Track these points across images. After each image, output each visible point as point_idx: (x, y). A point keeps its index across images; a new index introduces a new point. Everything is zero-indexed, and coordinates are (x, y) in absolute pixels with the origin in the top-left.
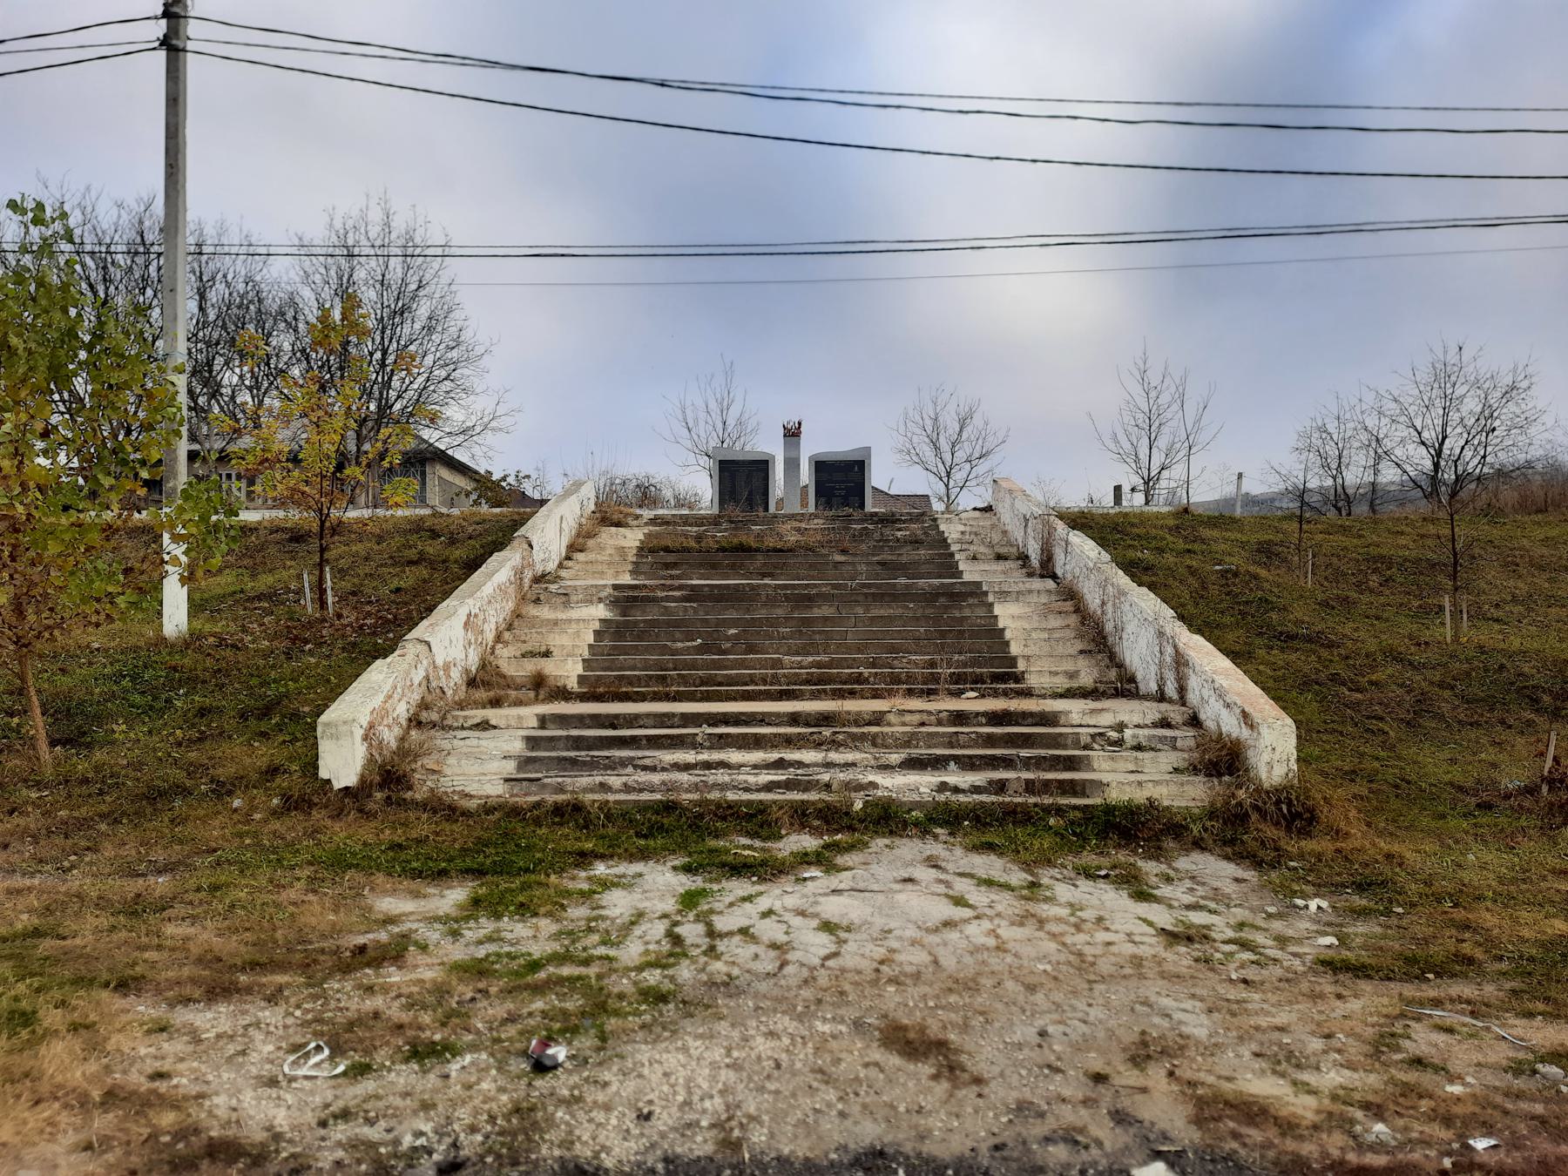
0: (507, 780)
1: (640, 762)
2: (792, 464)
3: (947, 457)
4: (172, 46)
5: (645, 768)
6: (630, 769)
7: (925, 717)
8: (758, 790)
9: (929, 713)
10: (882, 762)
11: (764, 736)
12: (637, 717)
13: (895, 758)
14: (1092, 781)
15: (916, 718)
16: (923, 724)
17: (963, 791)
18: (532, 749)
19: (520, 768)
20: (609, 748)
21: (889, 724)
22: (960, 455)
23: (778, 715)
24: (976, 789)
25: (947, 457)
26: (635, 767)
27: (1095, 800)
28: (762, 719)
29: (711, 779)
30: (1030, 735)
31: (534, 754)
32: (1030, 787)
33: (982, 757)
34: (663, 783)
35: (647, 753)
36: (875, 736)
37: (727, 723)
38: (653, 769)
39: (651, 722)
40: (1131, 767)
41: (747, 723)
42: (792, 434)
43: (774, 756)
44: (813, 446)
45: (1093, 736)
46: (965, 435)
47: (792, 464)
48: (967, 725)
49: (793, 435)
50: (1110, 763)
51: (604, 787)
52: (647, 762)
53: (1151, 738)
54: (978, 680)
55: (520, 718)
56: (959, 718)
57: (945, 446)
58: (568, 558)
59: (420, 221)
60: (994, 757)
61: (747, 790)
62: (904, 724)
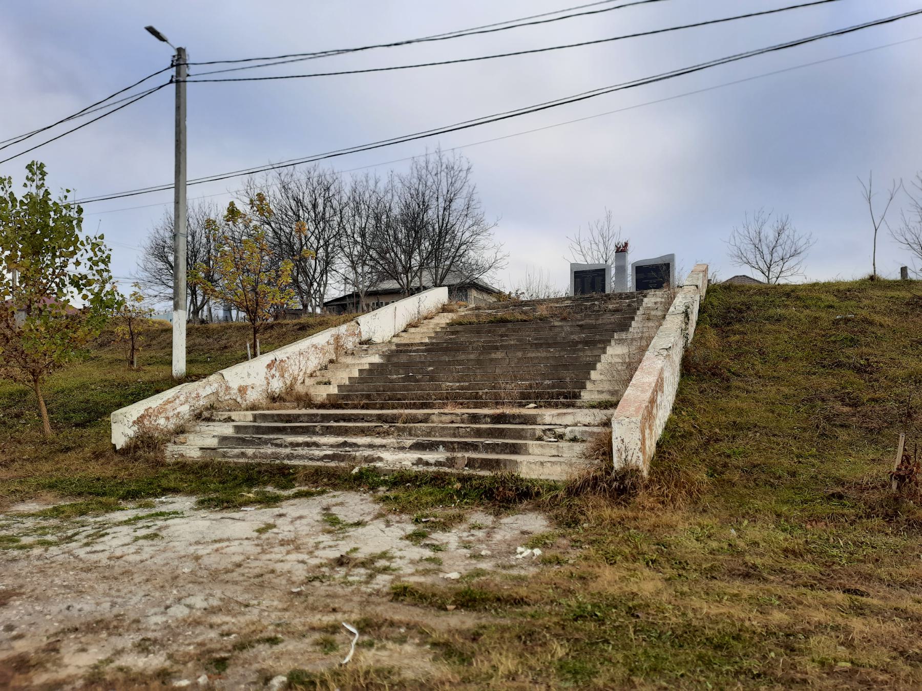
0: (201, 449)
1: (275, 442)
2: (621, 270)
3: (768, 258)
4: (178, 82)
5: (277, 445)
6: (269, 445)
7: (454, 418)
8: (318, 460)
9: (457, 415)
10: (401, 445)
11: (350, 427)
12: (299, 416)
13: (409, 442)
14: (510, 461)
15: (448, 418)
16: (452, 422)
17: (431, 465)
18: (237, 433)
19: (219, 443)
20: (272, 433)
21: (433, 422)
22: (776, 257)
23: (371, 415)
24: (438, 464)
25: (768, 258)
26: (272, 444)
27: (506, 473)
28: (362, 418)
29: (295, 453)
30: (503, 429)
31: (239, 435)
32: (471, 463)
33: (459, 443)
34: (273, 454)
35: (280, 436)
36: (411, 429)
37: (345, 420)
38: (279, 446)
39: (306, 419)
40: (554, 452)
41: (355, 421)
42: (622, 250)
43: (341, 439)
44: (634, 257)
45: (544, 431)
46: (780, 241)
47: (621, 270)
48: (479, 423)
49: (622, 251)
50: (540, 449)
51: (243, 455)
52: (278, 442)
53: (583, 433)
54: (538, 396)
55: (245, 415)
56: (474, 418)
57: (766, 251)
58: (405, 331)
59: (457, 157)
60: (466, 444)
61: (311, 459)
62: (441, 422)
